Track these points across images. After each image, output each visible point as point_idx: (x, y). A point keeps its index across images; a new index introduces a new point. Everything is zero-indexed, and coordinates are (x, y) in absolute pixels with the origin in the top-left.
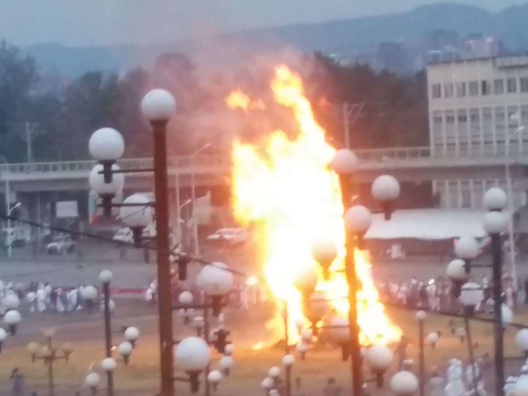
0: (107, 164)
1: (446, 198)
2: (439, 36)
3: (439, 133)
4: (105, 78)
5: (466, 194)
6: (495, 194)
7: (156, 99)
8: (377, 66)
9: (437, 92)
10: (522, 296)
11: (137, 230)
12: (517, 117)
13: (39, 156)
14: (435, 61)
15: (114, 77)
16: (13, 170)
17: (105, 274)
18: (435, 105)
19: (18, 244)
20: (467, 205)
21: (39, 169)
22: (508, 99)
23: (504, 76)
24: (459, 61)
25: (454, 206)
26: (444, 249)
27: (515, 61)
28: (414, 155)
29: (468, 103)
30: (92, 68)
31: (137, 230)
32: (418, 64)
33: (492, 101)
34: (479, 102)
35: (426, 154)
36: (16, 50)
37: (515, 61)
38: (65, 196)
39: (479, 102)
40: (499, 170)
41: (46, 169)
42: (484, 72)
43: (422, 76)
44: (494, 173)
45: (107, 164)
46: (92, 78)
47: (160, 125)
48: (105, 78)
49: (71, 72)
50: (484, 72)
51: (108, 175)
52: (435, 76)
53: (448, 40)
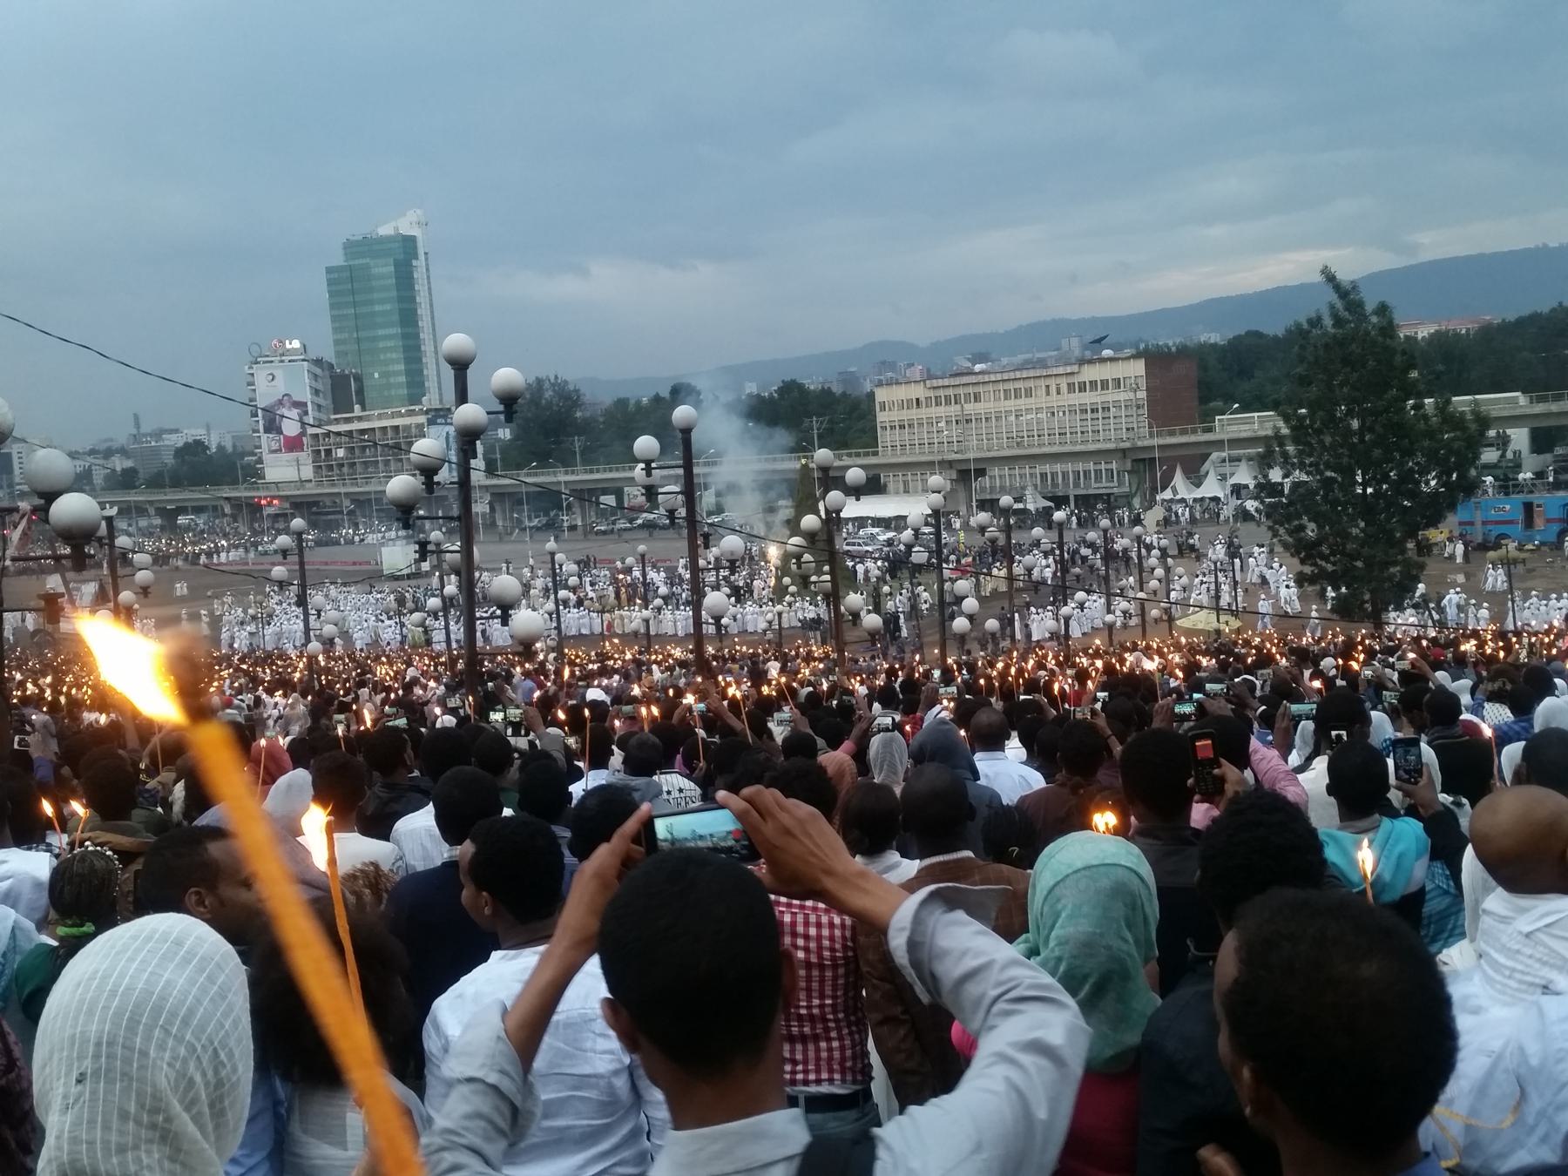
0: (648, 463)
1: (891, 486)
2: (885, 365)
3: (885, 438)
4: (632, 402)
5: (906, 483)
6: (935, 480)
7: (682, 413)
8: (837, 389)
9: (883, 408)
10: (99, 864)
11: (671, 513)
12: (942, 424)
13: (585, 462)
14: (880, 384)
15: (638, 402)
16: (566, 473)
17: (642, 548)
18: (882, 417)
19: (573, 528)
20: (906, 491)
21: (586, 472)
22: (935, 411)
23: (931, 394)
24: (898, 383)
25: (897, 493)
26: (898, 523)
27: (940, 382)
28: (867, 454)
29: (905, 415)
30: (622, 395)
31: (671, 513)
32: (868, 387)
33: (924, 413)
34: (914, 414)
35: (876, 454)
36: (566, 382)
37: (940, 382)
38: (605, 492)
39: (914, 414)
40: (932, 463)
41: (591, 471)
42: (918, 391)
43: (871, 396)
44: (929, 466)
45: (648, 463)
46: (622, 403)
47: (687, 432)
48: (632, 402)
49: (606, 399)
50: (918, 391)
51: (648, 471)
52: (881, 395)
53: (890, 366)
